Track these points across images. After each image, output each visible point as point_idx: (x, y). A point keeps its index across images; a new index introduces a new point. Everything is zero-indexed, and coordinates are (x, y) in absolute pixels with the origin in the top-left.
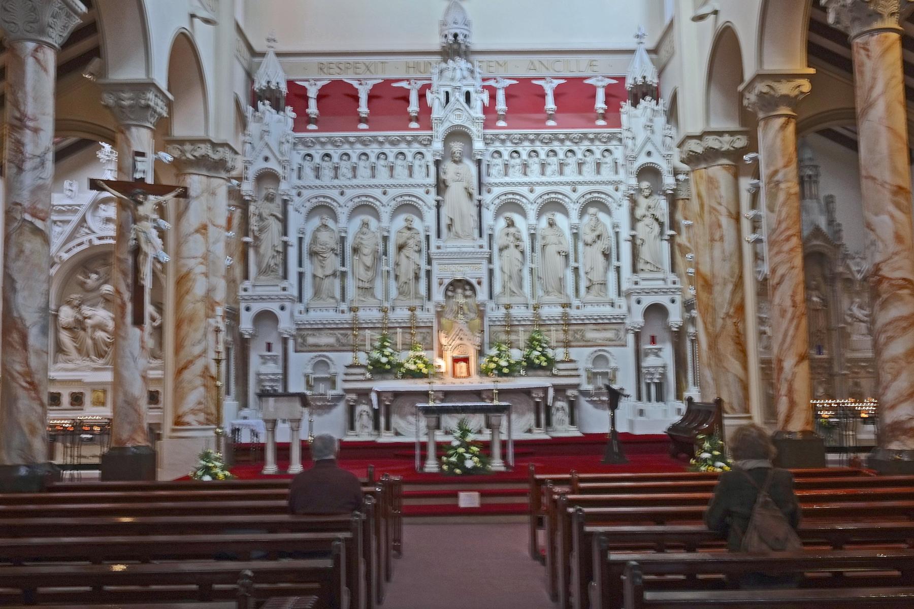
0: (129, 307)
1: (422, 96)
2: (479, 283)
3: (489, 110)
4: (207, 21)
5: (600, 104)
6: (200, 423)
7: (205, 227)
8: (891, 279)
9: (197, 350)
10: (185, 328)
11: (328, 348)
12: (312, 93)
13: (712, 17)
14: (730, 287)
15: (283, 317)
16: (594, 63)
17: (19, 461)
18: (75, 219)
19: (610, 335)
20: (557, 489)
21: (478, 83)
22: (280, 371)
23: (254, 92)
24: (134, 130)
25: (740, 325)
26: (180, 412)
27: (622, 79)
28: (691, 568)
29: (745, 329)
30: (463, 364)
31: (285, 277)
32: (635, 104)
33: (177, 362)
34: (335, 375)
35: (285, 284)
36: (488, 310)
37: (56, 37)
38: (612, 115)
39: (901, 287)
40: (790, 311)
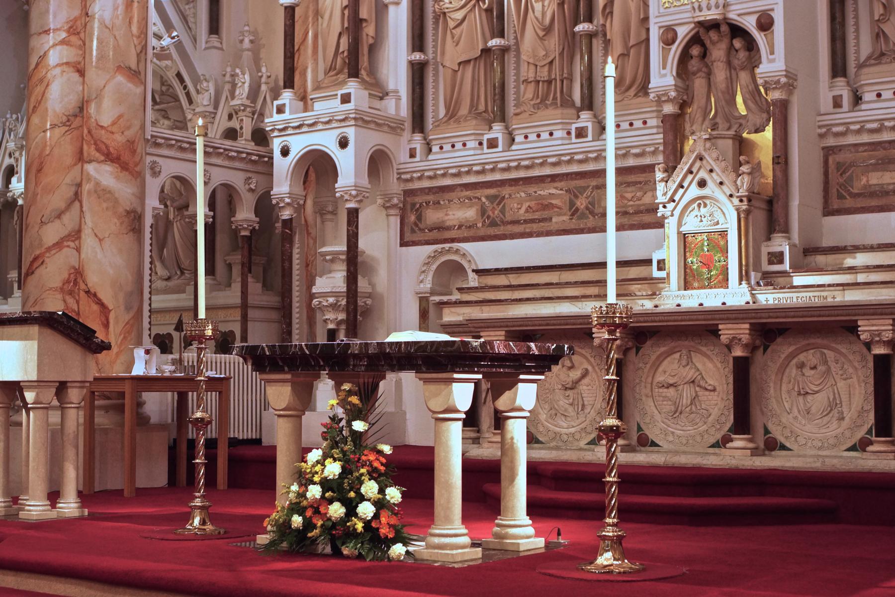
2: (765, 24)
9: (51, 233)
11: (465, 233)
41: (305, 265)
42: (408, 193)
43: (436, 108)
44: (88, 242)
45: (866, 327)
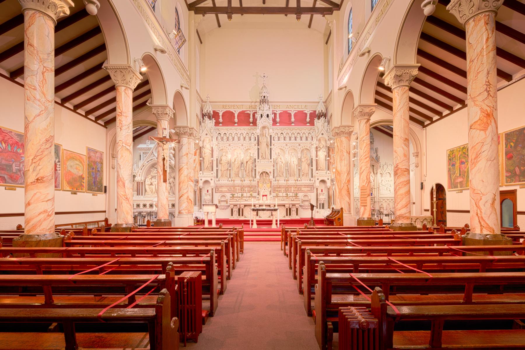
0: (162, 177)
1: (254, 116)
2: (270, 173)
3: (274, 121)
4: (186, 88)
5: (308, 119)
6: (186, 213)
7: (187, 154)
8: (401, 169)
9: (185, 191)
10: (181, 185)
11: (225, 192)
12: (221, 114)
13: (344, 89)
14: (346, 174)
15: (212, 182)
16: (306, 106)
17: (124, 223)
18: (150, 152)
19: (309, 189)
20: (292, 233)
21: (271, 112)
22: (211, 198)
23: (203, 114)
24: (162, 121)
25: (349, 186)
26: (180, 210)
27: (315, 111)
28: (356, 263)
29: (350, 187)
30: (266, 197)
31: (212, 170)
32: (319, 119)
33: (179, 195)
34: (227, 200)
35: (212, 172)
36: (273, 181)
37: (134, 86)
38: (312, 123)
39: (405, 172)
40: (366, 180)
41: (40, 185)
42: (216, 186)
43: (219, 175)
44: (189, 192)
45: (286, 206)
